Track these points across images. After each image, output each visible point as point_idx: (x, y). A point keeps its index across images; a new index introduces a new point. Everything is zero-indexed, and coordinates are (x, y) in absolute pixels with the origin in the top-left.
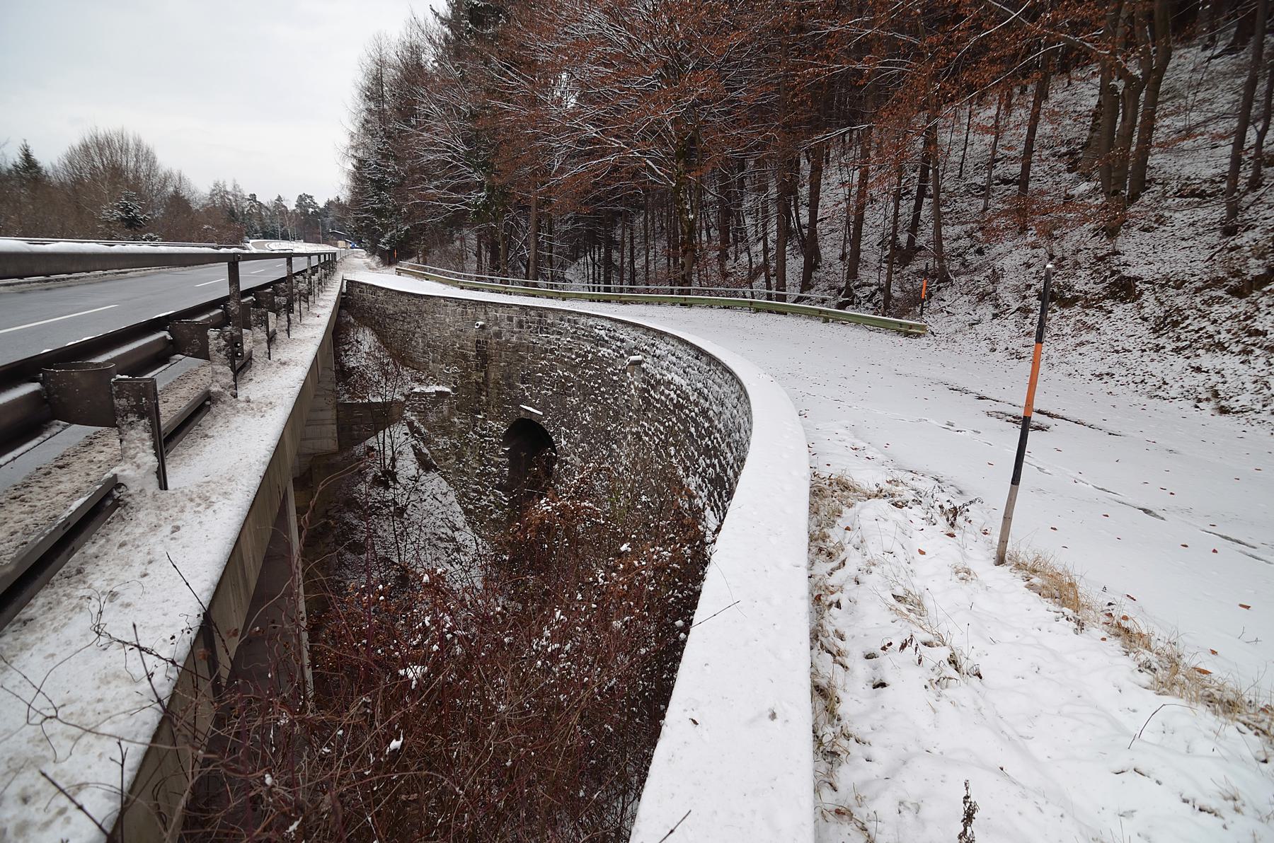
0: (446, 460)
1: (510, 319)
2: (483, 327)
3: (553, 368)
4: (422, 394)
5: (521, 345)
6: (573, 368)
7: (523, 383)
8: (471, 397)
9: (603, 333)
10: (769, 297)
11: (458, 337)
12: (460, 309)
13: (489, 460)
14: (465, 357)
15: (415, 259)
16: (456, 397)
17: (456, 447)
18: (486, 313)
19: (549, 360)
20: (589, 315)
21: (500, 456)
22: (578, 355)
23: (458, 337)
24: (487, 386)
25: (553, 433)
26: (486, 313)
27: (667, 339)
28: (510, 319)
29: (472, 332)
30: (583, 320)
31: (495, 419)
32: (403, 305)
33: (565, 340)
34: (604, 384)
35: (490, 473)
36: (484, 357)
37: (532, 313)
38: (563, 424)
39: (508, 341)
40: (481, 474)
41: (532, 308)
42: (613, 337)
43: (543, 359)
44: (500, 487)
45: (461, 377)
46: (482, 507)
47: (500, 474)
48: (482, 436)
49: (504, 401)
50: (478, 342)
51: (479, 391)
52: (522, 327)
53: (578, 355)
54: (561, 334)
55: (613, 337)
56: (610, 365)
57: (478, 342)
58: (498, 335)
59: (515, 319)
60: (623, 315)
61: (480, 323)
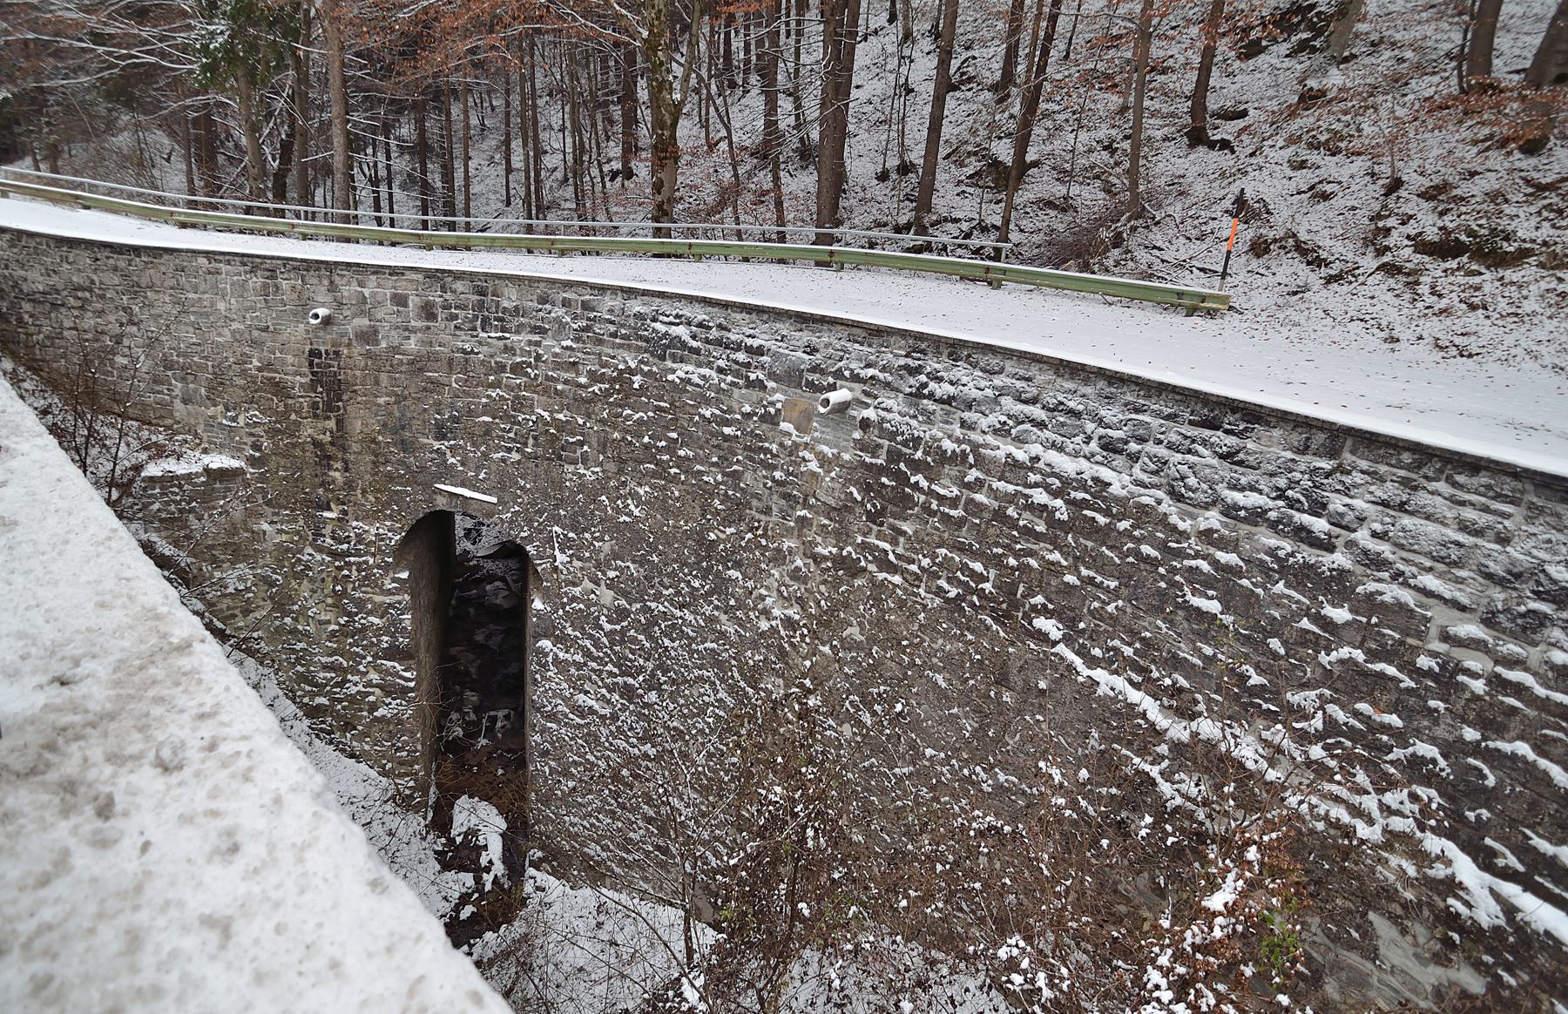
0: (247, 612)
1: (400, 300)
2: (327, 321)
3: (520, 404)
4: (168, 480)
5: (433, 358)
6: (585, 404)
7: (441, 436)
8: (304, 476)
9: (681, 331)
10: (379, 221)
11: (254, 343)
12: (256, 281)
13: (361, 604)
14: (280, 389)
15: (28, 160)
16: (262, 478)
17: (272, 584)
18: (332, 287)
19: (510, 388)
20: (630, 293)
21: (390, 592)
22: (594, 378)
23: (254, 343)
24: (344, 449)
25: (529, 539)
26: (332, 287)
27: (984, 360)
28: (400, 300)
29: (295, 333)
30: (609, 302)
31: (372, 517)
32: (79, 270)
33: (551, 346)
34: (687, 439)
35: (364, 628)
36: (330, 386)
37: (459, 286)
38: (557, 520)
39: (395, 350)
40: (344, 632)
41: (458, 276)
42: (719, 342)
43: (492, 386)
44: (393, 653)
45: (272, 433)
46: (352, 699)
47: (393, 628)
48: (335, 555)
49: (390, 478)
50: (314, 353)
51: (325, 460)
52: (431, 316)
53: (594, 378)
54: (542, 331)
55: (719, 342)
56: (708, 402)
57: (314, 353)
58: (369, 336)
59: (413, 302)
60: (753, 293)
61: (322, 312)
